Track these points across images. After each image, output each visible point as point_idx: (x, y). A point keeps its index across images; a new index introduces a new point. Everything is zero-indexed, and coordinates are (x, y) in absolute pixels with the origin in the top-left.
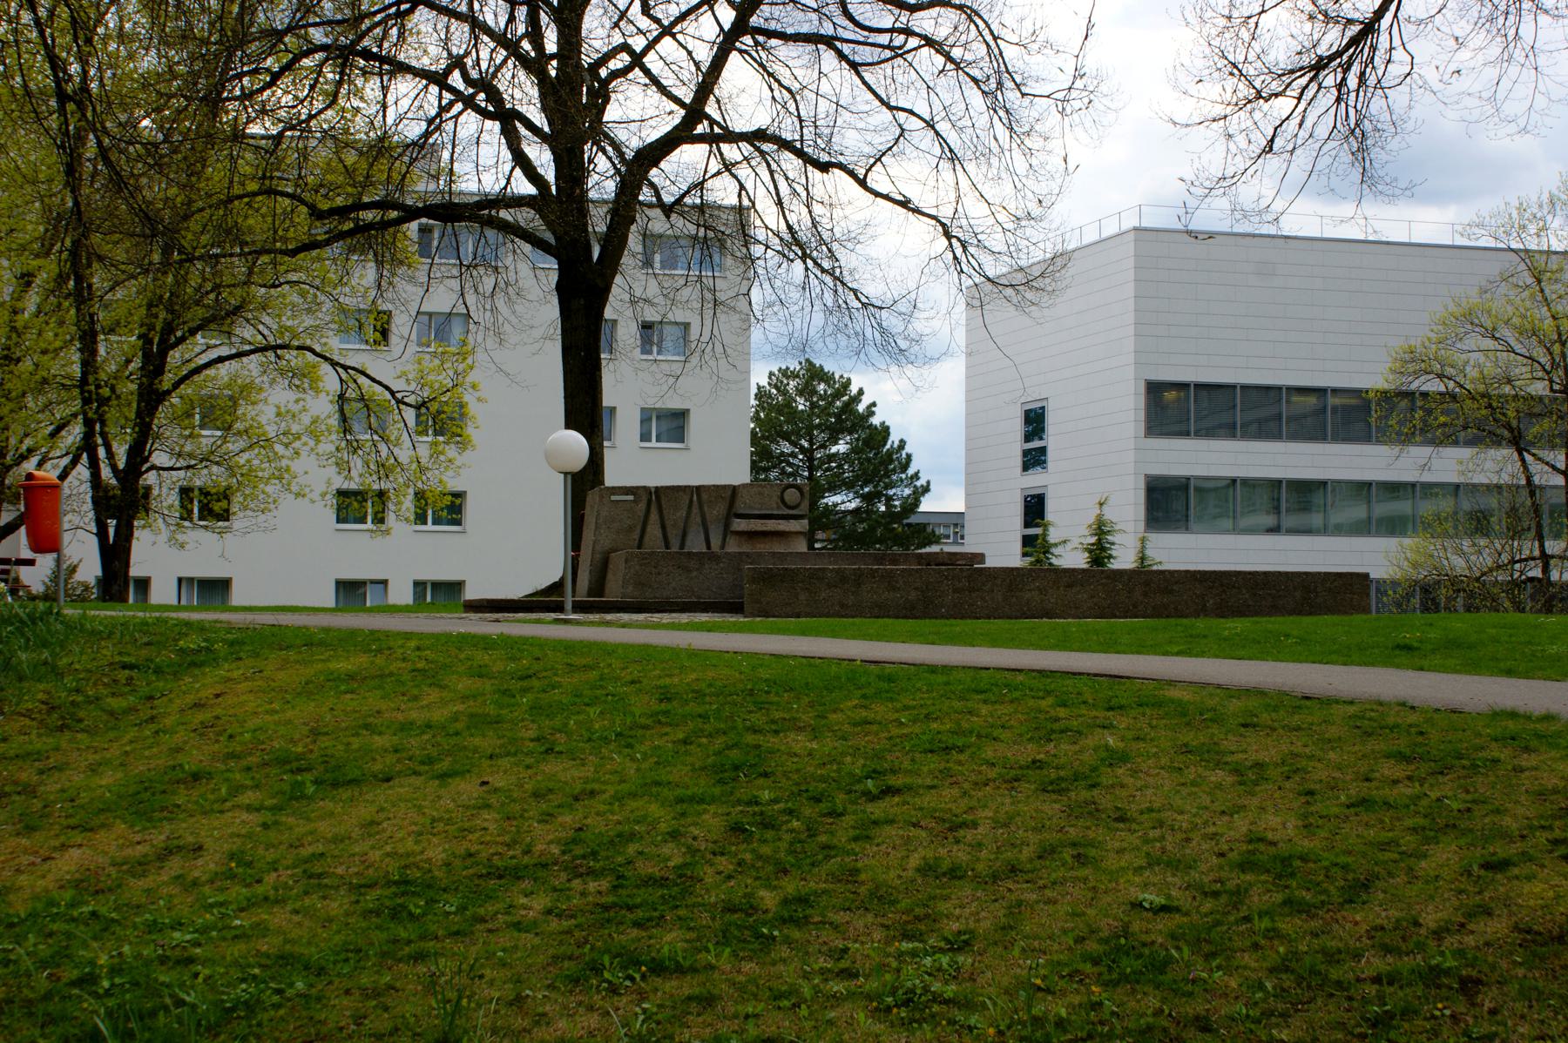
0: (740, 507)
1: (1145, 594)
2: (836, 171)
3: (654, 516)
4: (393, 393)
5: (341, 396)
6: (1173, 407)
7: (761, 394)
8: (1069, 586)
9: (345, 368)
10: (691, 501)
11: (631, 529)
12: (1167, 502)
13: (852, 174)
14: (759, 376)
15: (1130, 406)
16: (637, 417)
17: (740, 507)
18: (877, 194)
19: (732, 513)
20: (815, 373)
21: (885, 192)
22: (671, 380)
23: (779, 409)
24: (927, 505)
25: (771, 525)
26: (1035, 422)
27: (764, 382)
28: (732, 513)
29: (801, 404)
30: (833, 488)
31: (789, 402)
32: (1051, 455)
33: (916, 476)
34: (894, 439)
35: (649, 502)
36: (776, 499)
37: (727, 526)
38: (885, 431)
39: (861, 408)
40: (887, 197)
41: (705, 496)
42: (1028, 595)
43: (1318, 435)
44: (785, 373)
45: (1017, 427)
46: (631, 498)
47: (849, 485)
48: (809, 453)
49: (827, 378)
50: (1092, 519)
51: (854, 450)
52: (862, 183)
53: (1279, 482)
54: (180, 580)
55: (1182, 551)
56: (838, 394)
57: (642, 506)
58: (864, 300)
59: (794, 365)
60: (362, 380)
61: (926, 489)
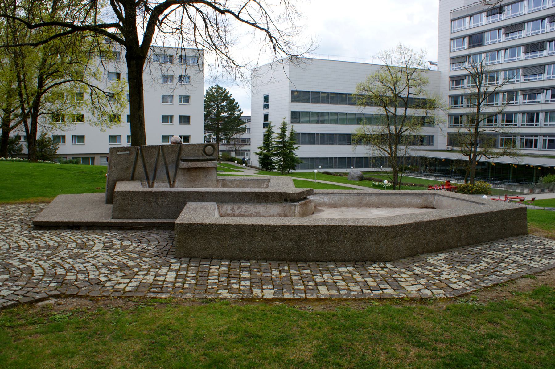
0: (183, 156)
1: (433, 236)
2: (226, 13)
3: (140, 161)
4: (105, 93)
5: (91, 94)
6: (297, 96)
7: (207, 92)
8: (394, 237)
9: (92, 86)
10: (159, 153)
11: (128, 168)
12: (296, 116)
13: (233, 14)
14: (206, 88)
15: (287, 96)
16: (178, 98)
17: (183, 156)
18: (243, 21)
19: (179, 159)
20: (219, 88)
21: (244, 23)
22: (172, 90)
23: (211, 95)
24: (242, 115)
25: (199, 164)
26: (266, 99)
27: (208, 89)
28: (179, 159)
29: (216, 94)
30: (223, 113)
31: (213, 94)
32: (270, 106)
33: (240, 110)
34: (236, 102)
35: (137, 154)
36: (201, 151)
37: (177, 165)
38: (234, 100)
39: (229, 95)
40: (247, 22)
41: (166, 150)
42: (368, 245)
43: (337, 103)
44: (212, 87)
45: (262, 99)
46: (127, 152)
47: (226, 112)
48: (217, 105)
49: (221, 89)
50: (282, 122)
51: (227, 104)
52: (237, 17)
53: (319, 112)
54: (72, 136)
55: (301, 128)
56: (224, 92)
57: (133, 156)
58: (236, 64)
59: (214, 86)
60: (97, 90)
61: (242, 113)
